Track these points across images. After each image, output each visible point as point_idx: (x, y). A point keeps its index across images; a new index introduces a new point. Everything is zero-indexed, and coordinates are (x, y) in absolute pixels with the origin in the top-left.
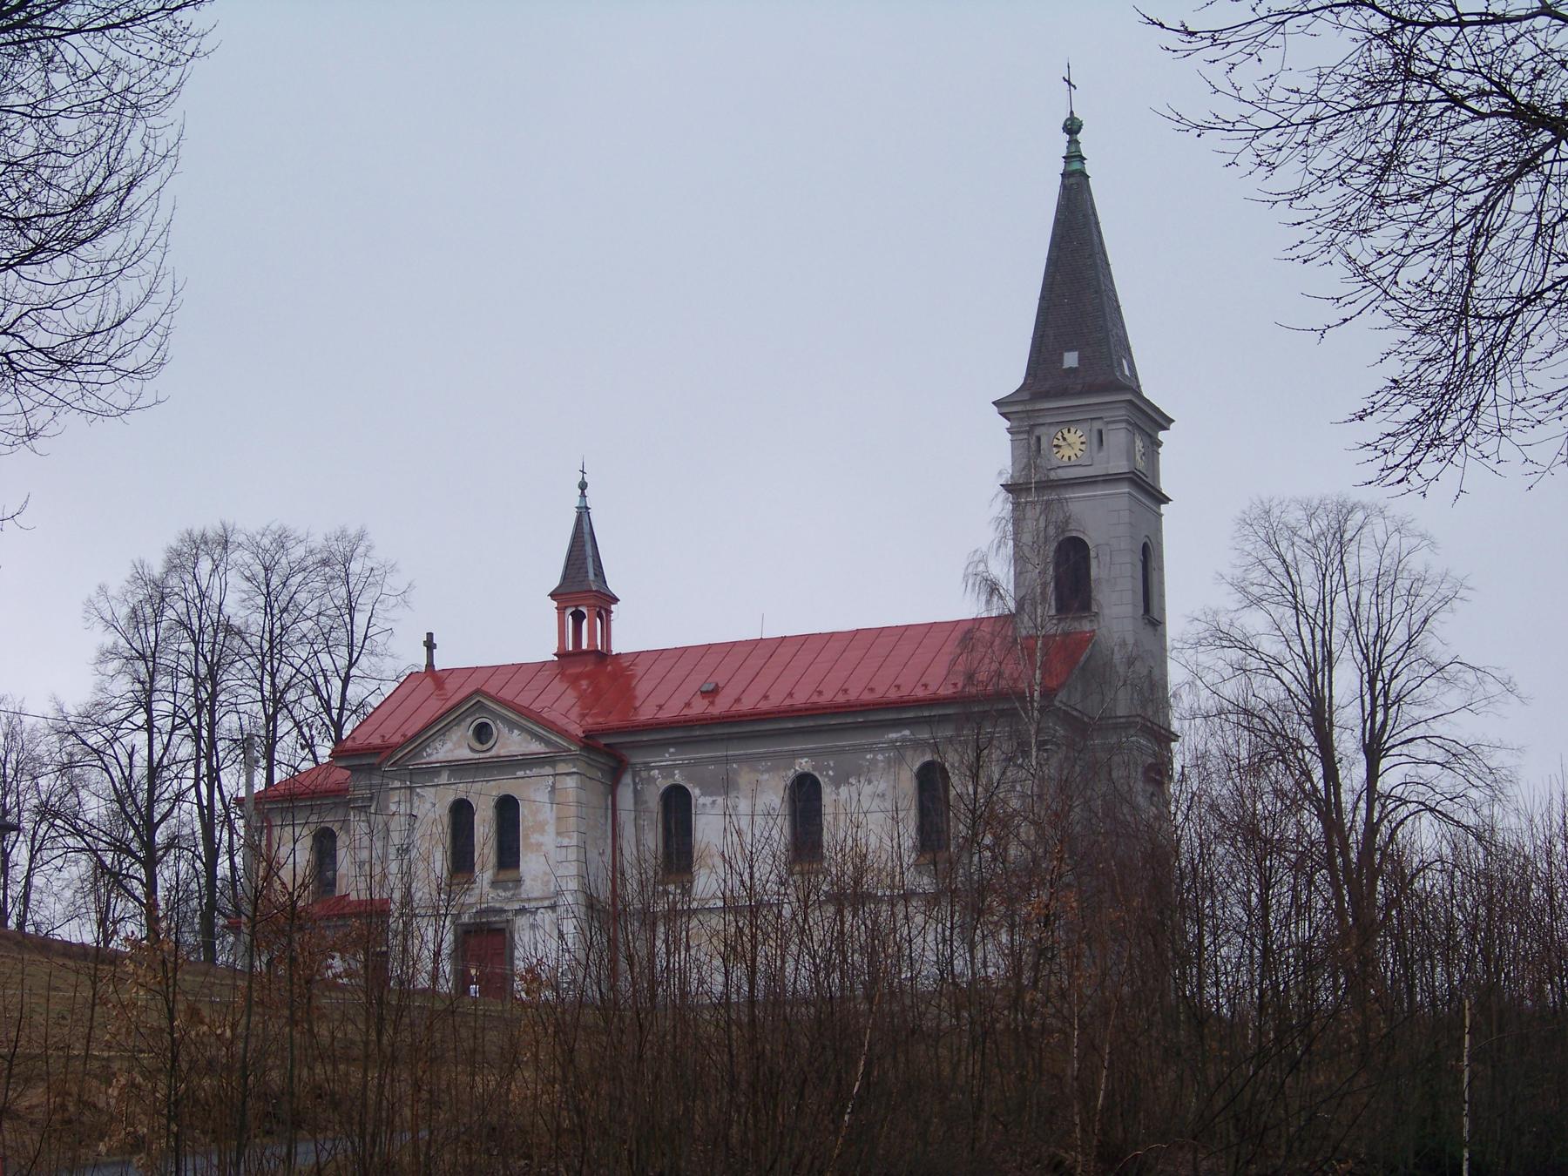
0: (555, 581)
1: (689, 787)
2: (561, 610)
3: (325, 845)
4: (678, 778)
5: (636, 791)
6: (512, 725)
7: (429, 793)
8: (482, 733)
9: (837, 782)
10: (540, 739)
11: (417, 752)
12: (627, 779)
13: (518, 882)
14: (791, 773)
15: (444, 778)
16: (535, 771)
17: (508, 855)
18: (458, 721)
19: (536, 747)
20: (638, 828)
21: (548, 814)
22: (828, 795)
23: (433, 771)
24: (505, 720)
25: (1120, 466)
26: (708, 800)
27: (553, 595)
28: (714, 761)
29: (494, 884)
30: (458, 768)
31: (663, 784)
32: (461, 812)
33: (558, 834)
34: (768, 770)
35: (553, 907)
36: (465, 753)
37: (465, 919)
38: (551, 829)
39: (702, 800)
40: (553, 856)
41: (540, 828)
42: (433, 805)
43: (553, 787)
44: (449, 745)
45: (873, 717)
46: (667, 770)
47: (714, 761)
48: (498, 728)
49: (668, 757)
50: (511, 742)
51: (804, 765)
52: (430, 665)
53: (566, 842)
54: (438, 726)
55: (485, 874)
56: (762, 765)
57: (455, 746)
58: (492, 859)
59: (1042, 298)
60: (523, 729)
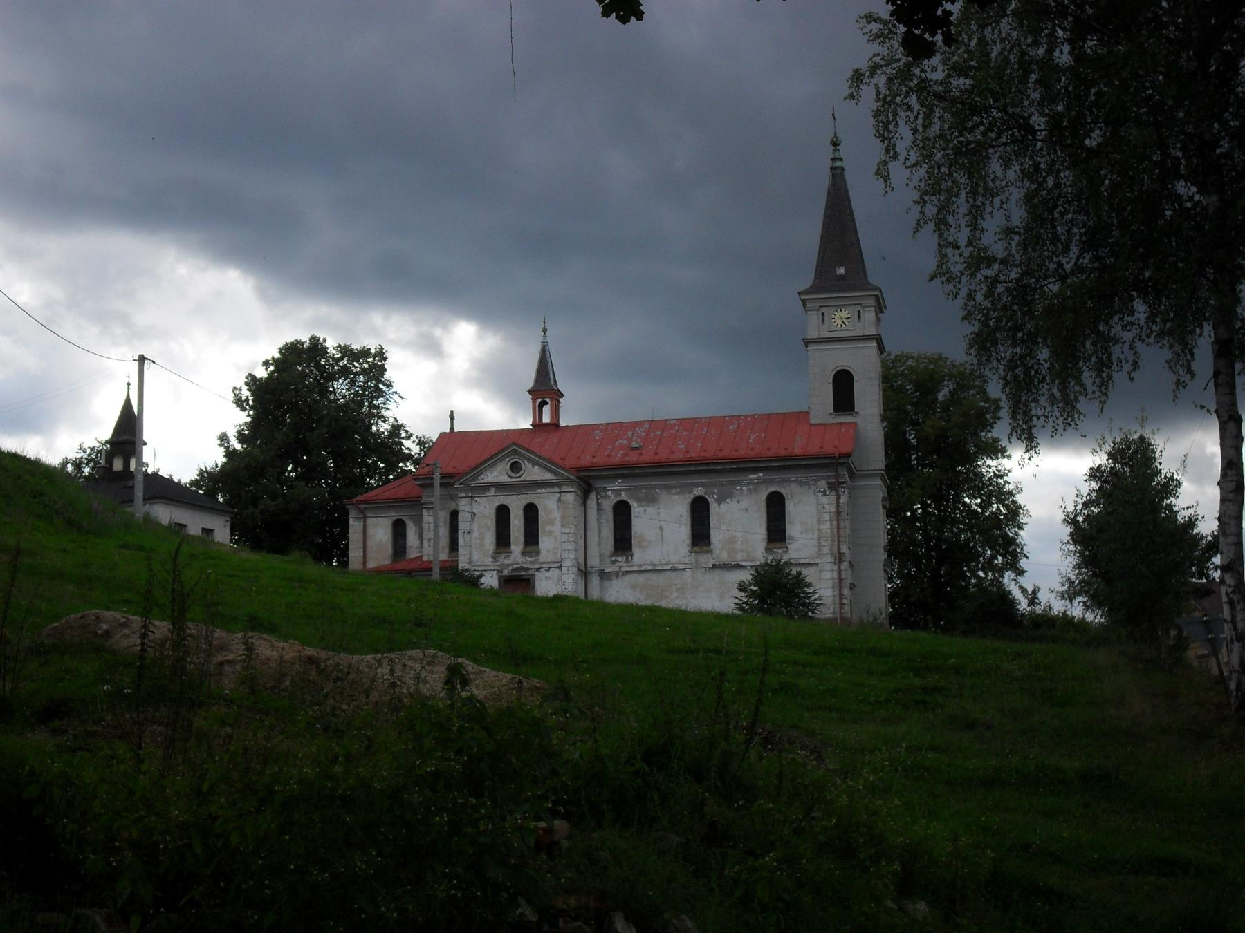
0: (530, 383)
1: (630, 501)
2: (534, 400)
3: (399, 529)
4: (624, 496)
5: (598, 503)
6: (534, 463)
7: (483, 501)
8: (515, 467)
9: (720, 501)
10: (552, 471)
11: (475, 478)
12: (593, 496)
13: (538, 552)
14: (692, 496)
15: (493, 490)
16: (549, 490)
17: (532, 537)
18: (501, 460)
19: (548, 476)
20: (600, 525)
21: (556, 515)
22: (714, 507)
23: (485, 488)
24: (530, 460)
25: (871, 331)
26: (641, 509)
27: (529, 392)
28: (645, 487)
29: (524, 553)
30: (501, 487)
31: (614, 500)
32: (503, 514)
33: (563, 526)
34: (678, 493)
35: (560, 567)
36: (505, 479)
37: (505, 573)
38: (558, 523)
39: (638, 510)
40: (556, 537)
41: (552, 522)
42: (485, 507)
43: (559, 500)
44: (495, 473)
45: (742, 466)
46: (617, 492)
47: (645, 487)
48: (526, 466)
49: (618, 484)
50: (533, 473)
51: (699, 491)
52: (452, 428)
53: (567, 530)
54: (491, 461)
55: (517, 547)
56: (674, 491)
57: (498, 474)
58: (522, 539)
59: (822, 236)
60: (540, 465)
